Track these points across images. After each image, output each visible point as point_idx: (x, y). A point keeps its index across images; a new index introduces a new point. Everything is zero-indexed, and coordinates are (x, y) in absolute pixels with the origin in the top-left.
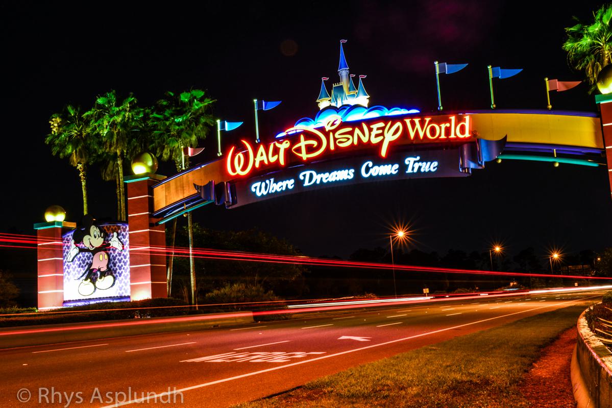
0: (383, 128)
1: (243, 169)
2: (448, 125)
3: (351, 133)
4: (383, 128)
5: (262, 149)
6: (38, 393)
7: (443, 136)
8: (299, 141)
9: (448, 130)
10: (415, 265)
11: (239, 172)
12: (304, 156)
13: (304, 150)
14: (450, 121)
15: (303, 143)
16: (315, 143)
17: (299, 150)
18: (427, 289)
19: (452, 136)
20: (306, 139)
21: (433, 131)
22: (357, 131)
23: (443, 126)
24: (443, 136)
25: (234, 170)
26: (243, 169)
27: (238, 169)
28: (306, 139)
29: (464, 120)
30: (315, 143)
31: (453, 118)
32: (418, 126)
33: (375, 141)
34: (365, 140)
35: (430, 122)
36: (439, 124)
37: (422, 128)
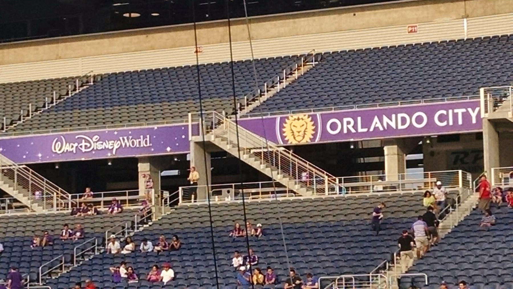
0: (113, 143)
1: (60, 150)
2: (140, 140)
3: (102, 144)
4: (113, 143)
5: (68, 144)
6: (187, 208)
7: (138, 146)
8: (81, 143)
9: (140, 142)
10: (244, 11)
11: (57, 151)
12: (83, 150)
13: (83, 147)
14: (140, 138)
15: (83, 144)
16: (89, 145)
17: (81, 146)
18: (166, 280)
19: (142, 146)
20: (85, 142)
21: (133, 142)
22: (104, 143)
23: (138, 140)
24: (138, 146)
25: (55, 149)
26: (60, 150)
27: (57, 149)
28: (85, 142)
29: (146, 138)
30: (89, 145)
31: (142, 137)
32: (126, 141)
33: (110, 148)
34: (107, 147)
35: (132, 139)
36: (136, 139)
37: (128, 141)
